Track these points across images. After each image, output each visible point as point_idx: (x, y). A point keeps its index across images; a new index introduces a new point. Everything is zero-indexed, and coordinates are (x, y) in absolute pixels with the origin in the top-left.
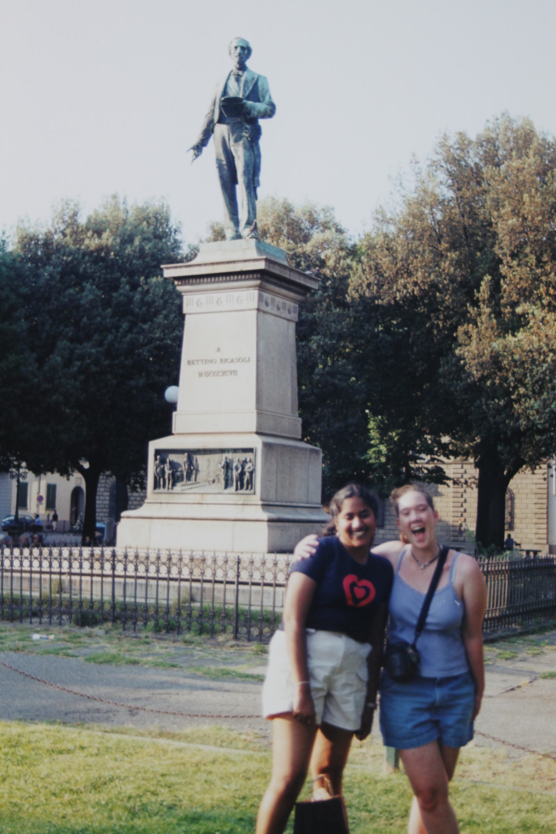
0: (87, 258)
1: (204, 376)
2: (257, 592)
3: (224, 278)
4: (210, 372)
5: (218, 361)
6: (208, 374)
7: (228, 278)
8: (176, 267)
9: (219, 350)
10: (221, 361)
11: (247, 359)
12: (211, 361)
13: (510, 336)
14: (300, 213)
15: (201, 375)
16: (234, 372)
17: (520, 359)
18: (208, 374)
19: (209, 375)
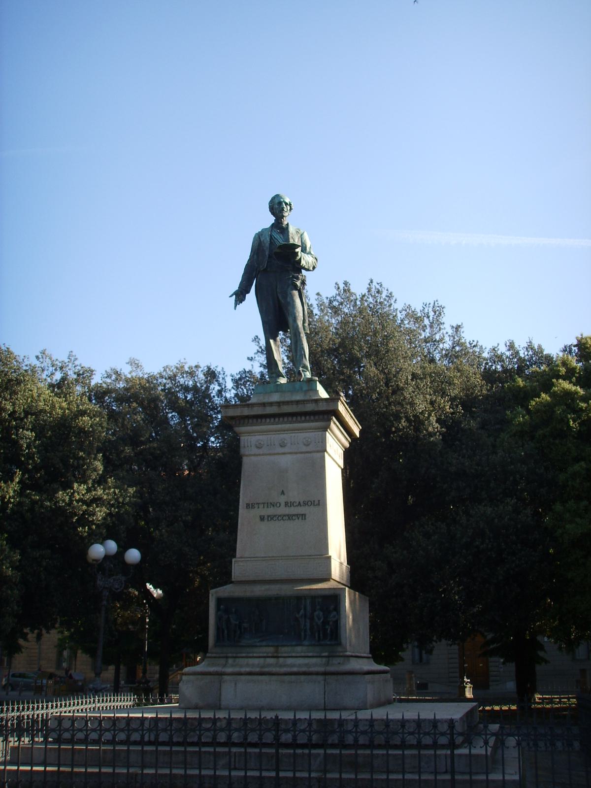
0: (31, 418)
1: (266, 520)
2: (413, 756)
3: (290, 419)
4: (275, 516)
5: (283, 504)
6: (271, 518)
7: (294, 419)
8: (356, 423)
9: (283, 493)
10: (286, 504)
11: (316, 502)
12: (273, 505)
13: (310, 262)
14: (561, 354)
15: (262, 518)
16: (303, 516)
17: (9, 563)
18: (271, 518)
19: (272, 519)
